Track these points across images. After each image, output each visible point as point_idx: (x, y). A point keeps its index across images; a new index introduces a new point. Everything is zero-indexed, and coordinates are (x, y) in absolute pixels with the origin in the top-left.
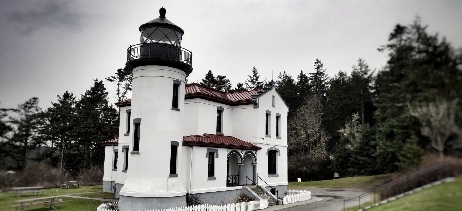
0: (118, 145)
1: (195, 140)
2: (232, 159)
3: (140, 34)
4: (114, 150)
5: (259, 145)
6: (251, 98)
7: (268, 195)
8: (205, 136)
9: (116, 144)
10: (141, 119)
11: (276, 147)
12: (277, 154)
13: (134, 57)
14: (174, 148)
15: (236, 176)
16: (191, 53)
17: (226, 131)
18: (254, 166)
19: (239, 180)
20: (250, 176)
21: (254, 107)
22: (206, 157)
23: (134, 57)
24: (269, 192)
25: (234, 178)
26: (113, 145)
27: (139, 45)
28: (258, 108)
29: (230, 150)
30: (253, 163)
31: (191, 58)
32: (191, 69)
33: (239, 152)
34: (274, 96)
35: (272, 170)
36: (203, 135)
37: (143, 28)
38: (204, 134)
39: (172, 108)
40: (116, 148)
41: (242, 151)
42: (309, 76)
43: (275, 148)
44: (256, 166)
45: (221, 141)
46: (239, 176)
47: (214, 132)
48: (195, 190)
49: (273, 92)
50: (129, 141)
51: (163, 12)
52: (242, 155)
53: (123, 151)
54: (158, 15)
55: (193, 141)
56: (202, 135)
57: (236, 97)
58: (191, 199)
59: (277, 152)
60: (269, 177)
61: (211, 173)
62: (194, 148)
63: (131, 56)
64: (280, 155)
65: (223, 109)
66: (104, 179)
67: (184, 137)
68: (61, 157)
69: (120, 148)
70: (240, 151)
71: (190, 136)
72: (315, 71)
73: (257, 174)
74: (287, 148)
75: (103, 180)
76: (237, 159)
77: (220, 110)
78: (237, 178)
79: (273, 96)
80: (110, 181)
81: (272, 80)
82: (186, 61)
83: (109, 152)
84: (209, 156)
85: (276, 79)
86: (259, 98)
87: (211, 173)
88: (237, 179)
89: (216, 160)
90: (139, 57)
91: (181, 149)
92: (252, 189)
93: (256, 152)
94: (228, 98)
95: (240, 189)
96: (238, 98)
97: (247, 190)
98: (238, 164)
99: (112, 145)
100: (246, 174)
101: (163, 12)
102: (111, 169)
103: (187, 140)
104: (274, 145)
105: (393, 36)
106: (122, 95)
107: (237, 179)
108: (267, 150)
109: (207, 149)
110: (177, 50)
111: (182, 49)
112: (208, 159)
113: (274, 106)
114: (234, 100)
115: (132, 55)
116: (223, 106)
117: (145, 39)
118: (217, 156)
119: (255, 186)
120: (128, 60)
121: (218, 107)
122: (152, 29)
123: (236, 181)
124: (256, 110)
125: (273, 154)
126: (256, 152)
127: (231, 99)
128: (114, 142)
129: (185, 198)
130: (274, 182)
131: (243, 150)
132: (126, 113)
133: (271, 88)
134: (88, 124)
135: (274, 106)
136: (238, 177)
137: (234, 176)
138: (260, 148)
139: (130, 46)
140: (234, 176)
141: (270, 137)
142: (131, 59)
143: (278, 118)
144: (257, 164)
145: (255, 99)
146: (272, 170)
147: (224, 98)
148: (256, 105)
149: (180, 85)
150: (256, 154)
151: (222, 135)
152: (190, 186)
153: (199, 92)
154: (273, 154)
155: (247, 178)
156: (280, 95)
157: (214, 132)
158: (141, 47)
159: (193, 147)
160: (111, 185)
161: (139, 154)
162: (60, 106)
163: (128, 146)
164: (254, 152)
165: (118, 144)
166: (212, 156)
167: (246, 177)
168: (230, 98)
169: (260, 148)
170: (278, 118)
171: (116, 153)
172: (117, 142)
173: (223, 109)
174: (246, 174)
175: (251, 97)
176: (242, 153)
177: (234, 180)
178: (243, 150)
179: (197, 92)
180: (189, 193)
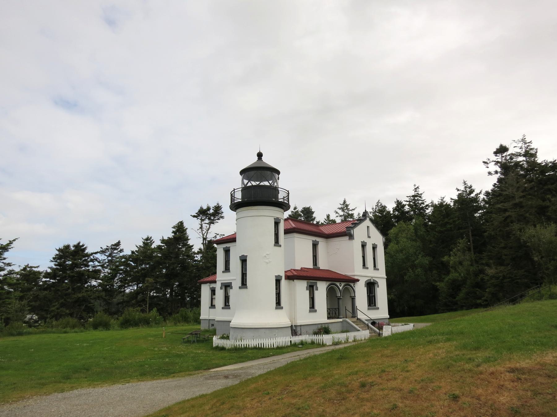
0: (216, 283)
1: (296, 274)
2: (331, 292)
3: (240, 177)
4: (211, 288)
5: (356, 278)
6: (346, 230)
7: (369, 328)
8: (302, 269)
9: (215, 282)
10: (247, 256)
11: (373, 278)
12: (376, 286)
13: (239, 199)
14: (278, 281)
15: (335, 309)
16: (288, 191)
17: (322, 265)
18: (353, 299)
19: (339, 313)
20: (350, 308)
21: (349, 239)
22: (307, 289)
23: (239, 199)
24: (370, 325)
25: (334, 310)
26: (209, 283)
27: (241, 189)
28: (353, 240)
29: (328, 283)
30: (352, 296)
31: (288, 196)
32: (289, 207)
33: (338, 285)
34: (369, 227)
35: (372, 302)
36: (301, 269)
37: (243, 172)
38: (302, 268)
39: (274, 244)
40: (213, 285)
41: (340, 283)
42: (404, 203)
43: (373, 280)
44: (354, 298)
45: (317, 274)
46: (338, 309)
47: (311, 266)
48: (299, 322)
49: (367, 223)
50: (234, 276)
51: (260, 155)
52: (341, 288)
53: (221, 288)
54: (257, 158)
55: (293, 274)
56: (300, 269)
57: (333, 229)
58: (294, 330)
59: (375, 285)
60: (368, 309)
61: (312, 307)
62: (295, 281)
63: (235, 199)
64: (378, 287)
65: (318, 242)
66: (201, 317)
67: (285, 272)
68: (147, 299)
69: (218, 286)
70: (338, 284)
71: (290, 270)
72: (413, 193)
73: (357, 306)
74: (385, 279)
75: (200, 318)
76: (335, 291)
77: (315, 243)
78: (337, 310)
79: (368, 227)
80: (208, 319)
81: (366, 211)
82: (282, 199)
83: (205, 290)
84: (310, 289)
85: (369, 210)
86: (354, 230)
87: (312, 307)
88: (337, 312)
89: (316, 293)
90: (241, 200)
91: (283, 282)
92: (352, 322)
93: (354, 284)
94: (321, 230)
95: (341, 322)
96: (333, 229)
97: (348, 323)
98: (337, 297)
99: (208, 283)
100: (345, 307)
101: (260, 155)
102: (209, 308)
103: (289, 274)
104: (372, 277)
105: (496, 153)
106: (205, 231)
107: (337, 312)
108: (365, 282)
109: (307, 282)
110: (275, 190)
111: (279, 189)
112: (308, 291)
113: (369, 237)
114: (328, 232)
115: (236, 198)
116: (318, 239)
117: (246, 181)
118: (317, 289)
119: (355, 319)
120: (231, 202)
121: (313, 241)
122: (252, 173)
123: (335, 313)
124: (351, 242)
125: (371, 286)
126: (354, 284)
127: (325, 232)
128: (210, 280)
129: (290, 329)
130: (374, 315)
131: (341, 283)
132: (223, 251)
133: (365, 219)
134: (536, 254)
135: (369, 237)
136: (337, 309)
137: (334, 309)
138: (358, 280)
139: (233, 190)
140: (334, 309)
141: (367, 268)
142: (235, 201)
143: (374, 248)
144: (355, 296)
145: (350, 231)
146: (372, 302)
147: (318, 231)
148: (351, 237)
149: (280, 223)
150: (354, 287)
151: (319, 269)
152: (293, 318)
153: (295, 227)
154: (371, 286)
155: (346, 310)
156: (375, 225)
157: (311, 266)
158: (242, 190)
159: (294, 280)
160: (209, 323)
161: (247, 288)
162: (163, 248)
163: (231, 282)
164: (352, 284)
165: (216, 281)
166: (311, 289)
167: (346, 309)
168: (324, 231)
169: (358, 280)
170: (374, 248)
171: (213, 291)
172: (215, 279)
173: (318, 242)
174: (345, 307)
175: (345, 229)
176: (340, 286)
177: (334, 313)
178: (341, 283)
179: (292, 227)
180: (293, 325)
